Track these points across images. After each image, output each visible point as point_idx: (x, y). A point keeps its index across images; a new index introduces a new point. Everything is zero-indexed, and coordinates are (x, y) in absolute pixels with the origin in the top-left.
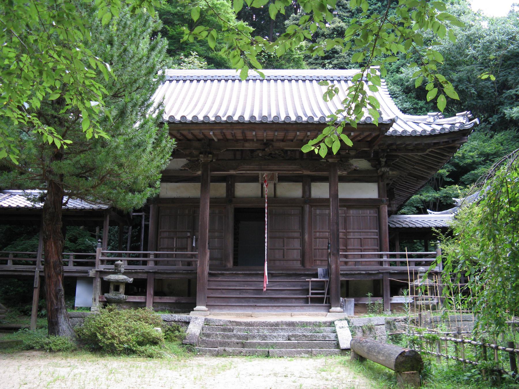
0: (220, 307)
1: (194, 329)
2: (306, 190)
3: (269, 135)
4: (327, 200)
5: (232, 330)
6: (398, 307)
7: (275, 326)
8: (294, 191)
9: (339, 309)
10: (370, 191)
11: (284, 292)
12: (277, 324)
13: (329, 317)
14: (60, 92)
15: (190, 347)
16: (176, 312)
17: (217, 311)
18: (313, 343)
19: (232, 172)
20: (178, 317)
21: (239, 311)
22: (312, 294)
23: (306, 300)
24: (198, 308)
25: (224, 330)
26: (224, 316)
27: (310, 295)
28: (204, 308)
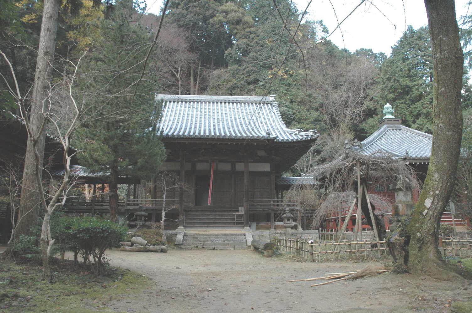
0: (190, 227)
1: (180, 237)
2: (233, 167)
3: (213, 143)
4: (243, 172)
5: (196, 238)
6: (276, 227)
7: (216, 236)
8: (227, 167)
9: (248, 228)
10: (266, 167)
11: (222, 219)
12: (218, 235)
13: (243, 232)
14: (135, 147)
15: (179, 246)
16: (170, 230)
17: (189, 229)
18: (234, 243)
19: (196, 160)
20: (171, 232)
21: (201, 229)
22: (236, 220)
23: (234, 223)
24: (179, 227)
25: (194, 238)
26: (192, 231)
27: (235, 221)
28: (182, 227)
